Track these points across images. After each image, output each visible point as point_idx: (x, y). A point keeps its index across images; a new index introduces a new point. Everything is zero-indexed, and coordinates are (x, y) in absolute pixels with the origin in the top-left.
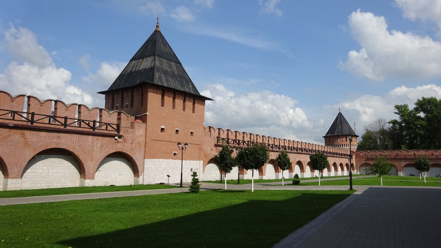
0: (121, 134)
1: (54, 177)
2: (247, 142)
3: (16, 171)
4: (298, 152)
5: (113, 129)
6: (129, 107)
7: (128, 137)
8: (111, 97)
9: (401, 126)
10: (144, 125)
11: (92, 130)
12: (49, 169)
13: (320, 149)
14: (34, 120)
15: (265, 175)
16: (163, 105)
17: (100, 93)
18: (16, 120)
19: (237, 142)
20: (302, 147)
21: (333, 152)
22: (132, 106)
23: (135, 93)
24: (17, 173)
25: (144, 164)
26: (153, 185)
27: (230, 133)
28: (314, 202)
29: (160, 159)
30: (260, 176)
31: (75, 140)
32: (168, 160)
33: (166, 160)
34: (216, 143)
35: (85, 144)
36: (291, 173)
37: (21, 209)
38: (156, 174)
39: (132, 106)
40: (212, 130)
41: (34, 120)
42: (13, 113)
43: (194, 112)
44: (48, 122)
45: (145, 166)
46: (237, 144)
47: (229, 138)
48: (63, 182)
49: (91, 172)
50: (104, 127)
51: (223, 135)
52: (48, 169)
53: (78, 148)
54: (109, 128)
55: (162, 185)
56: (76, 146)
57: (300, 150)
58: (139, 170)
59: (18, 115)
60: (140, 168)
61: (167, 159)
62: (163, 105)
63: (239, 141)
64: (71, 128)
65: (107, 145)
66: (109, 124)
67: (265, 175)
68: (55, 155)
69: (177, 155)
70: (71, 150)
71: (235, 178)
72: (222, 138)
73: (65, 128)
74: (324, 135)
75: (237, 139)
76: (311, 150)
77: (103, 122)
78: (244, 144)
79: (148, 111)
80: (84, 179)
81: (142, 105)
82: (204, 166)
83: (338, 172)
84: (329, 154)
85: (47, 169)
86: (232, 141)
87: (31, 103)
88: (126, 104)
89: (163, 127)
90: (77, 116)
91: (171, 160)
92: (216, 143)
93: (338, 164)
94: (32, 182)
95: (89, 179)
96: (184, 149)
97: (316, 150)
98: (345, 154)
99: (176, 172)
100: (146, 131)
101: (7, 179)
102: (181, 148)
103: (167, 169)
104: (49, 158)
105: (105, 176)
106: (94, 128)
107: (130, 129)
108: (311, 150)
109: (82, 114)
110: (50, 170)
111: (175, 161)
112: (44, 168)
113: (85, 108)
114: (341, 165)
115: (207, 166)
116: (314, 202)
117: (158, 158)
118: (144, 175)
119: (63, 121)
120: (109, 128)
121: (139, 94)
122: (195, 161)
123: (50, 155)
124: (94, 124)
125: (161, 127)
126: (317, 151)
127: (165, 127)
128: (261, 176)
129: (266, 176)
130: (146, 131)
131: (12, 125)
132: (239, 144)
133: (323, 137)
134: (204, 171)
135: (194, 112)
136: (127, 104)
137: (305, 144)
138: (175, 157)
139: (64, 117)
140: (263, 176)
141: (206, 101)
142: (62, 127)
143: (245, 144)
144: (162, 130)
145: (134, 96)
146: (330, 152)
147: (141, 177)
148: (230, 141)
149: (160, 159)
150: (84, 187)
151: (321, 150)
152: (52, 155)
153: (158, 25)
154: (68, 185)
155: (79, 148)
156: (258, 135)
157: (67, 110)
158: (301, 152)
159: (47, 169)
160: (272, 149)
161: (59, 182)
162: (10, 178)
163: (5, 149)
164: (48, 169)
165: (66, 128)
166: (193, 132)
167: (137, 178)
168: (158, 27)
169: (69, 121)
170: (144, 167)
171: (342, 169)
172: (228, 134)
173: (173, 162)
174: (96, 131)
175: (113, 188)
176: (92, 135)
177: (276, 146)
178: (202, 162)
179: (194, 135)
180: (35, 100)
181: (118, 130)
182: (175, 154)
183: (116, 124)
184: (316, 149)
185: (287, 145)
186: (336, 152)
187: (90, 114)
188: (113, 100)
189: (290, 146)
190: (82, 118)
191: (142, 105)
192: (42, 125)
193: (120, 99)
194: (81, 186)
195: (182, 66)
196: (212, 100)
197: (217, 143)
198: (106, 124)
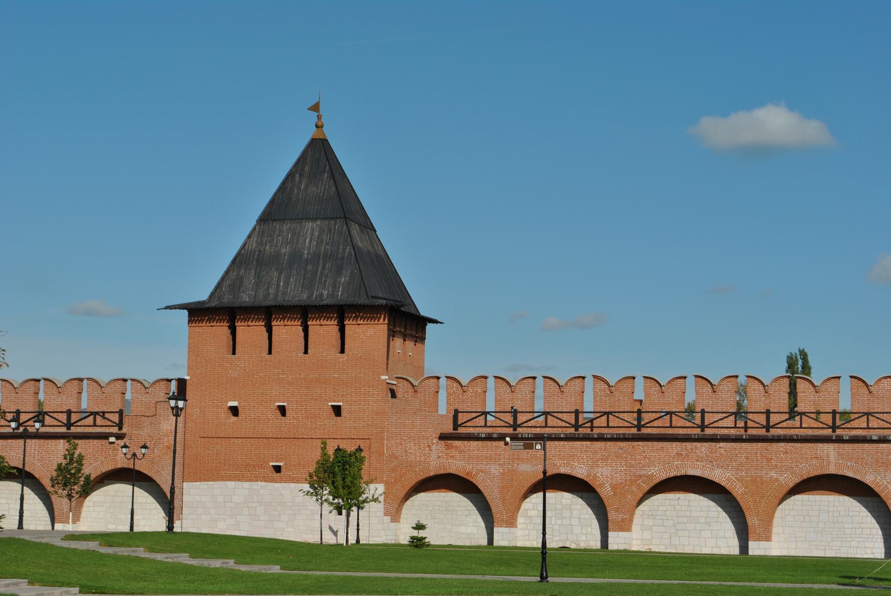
7: (142, 436)
12: (9, 504)
14: (580, 424)
26: (446, 545)
29: (227, 482)
31: (33, 450)
33: (248, 483)
35: (51, 457)
37: (210, 572)
38: (217, 516)
41: (72, 422)
43: (270, 353)
44: (92, 423)
49: (65, 510)
52: (850, 516)
53: (39, 464)
56: (34, 462)
61: (249, 481)
65: (94, 455)
69: (283, 470)
88: (398, 351)
89: (235, 404)
91: (263, 484)
95: (61, 523)
99: (279, 515)
103: (250, 505)
104: (117, 483)
105: (112, 520)
107: (146, 418)
113: (95, 383)
115: (780, 506)
117: (223, 480)
119: (762, 419)
125: (227, 405)
127: (239, 403)
131: (848, 438)
135: (270, 353)
139: (118, 410)
144: (235, 411)
149: (227, 482)
153: (320, 124)
155: (40, 465)
157: (60, 393)
159: (7, 503)
162: (611, 531)
164: (850, 516)
165: (515, 432)
166: (340, 406)
168: (322, 127)
173: (270, 488)
176: (63, 439)
182: (278, 469)
187: (104, 394)
196: (441, 323)
197: (455, 428)
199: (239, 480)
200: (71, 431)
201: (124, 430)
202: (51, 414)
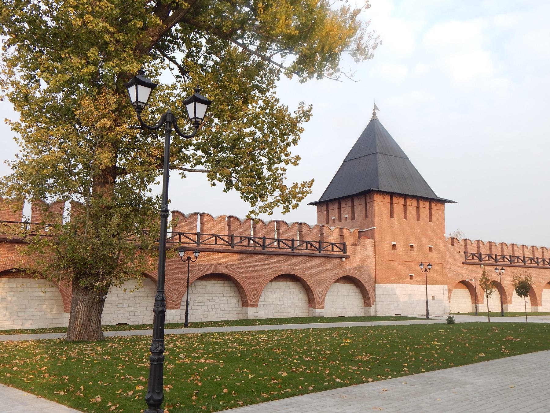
0: (348, 254)
1: (285, 306)
2: (509, 258)
6: (349, 220)
8: (324, 208)
9: (136, 73)
10: (371, 241)
11: (196, 245)
15: (541, 305)
16: (392, 215)
17: (310, 204)
18: (281, 248)
22: (353, 218)
25: (375, 291)
27: (481, 245)
30: (533, 307)
34: (464, 261)
38: (390, 302)
39: (353, 218)
40: (455, 242)
43: (430, 220)
44: (331, 250)
45: (377, 293)
46: (493, 260)
47: (526, 256)
48: (293, 311)
51: (472, 250)
55: (397, 317)
57: (475, 258)
58: (371, 298)
59: (289, 245)
60: (371, 295)
62: (392, 215)
63: (496, 255)
64: (325, 252)
66: (182, 234)
67: (541, 305)
69: (414, 278)
70: (299, 275)
71: (494, 310)
78: (544, 263)
79: (376, 224)
81: (366, 217)
82: (450, 291)
86: (471, 255)
87: (205, 221)
88: (345, 216)
89: (394, 243)
90: (276, 236)
91: (407, 285)
92: (464, 261)
94: (266, 311)
96: (428, 270)
100: (375, 249)
101: (246, 308)
102: (424, 270)
106: (293, 248)
109: (304, 233)
110: (281, 299)
112: (276, 296)
118: (376, 304)
119: (290, 243)
122: (437, 286)
124: (293, 244)
128: (536, 307)
129: (543, 306)
130: (375, 249)
132: (496, 260)
134: (449, 299)
135: (430, 220)
136: (347, 216)
137: (523, 248)
138: (411, 280)
140: (508, 305)
142: (317, 252)
143: (506, 260)
145: (355, 207)
147: (373, 306)
154: (298, 314)
156: (525, 246)
160: (538, 265)
161: (289, 311)
169: (267, 242)
170: (375, 295)
174: (295, 251)
175: (341, 318)
177: (518, 258)
178: (446, 287)
179: (434, 251)
181: (344, 250)
184: (524, 254)
185: (528, 254)
188: (328, 211)
189: (494, 253)
190: (305, 239)
191: (366, 217)
192: (272, 250)
193: (337, 210)
195: (409, 161)
196: (454, 202)
197: (465, 260)
199: (398, 283)
200: (234, 249)
202: (284, 241)
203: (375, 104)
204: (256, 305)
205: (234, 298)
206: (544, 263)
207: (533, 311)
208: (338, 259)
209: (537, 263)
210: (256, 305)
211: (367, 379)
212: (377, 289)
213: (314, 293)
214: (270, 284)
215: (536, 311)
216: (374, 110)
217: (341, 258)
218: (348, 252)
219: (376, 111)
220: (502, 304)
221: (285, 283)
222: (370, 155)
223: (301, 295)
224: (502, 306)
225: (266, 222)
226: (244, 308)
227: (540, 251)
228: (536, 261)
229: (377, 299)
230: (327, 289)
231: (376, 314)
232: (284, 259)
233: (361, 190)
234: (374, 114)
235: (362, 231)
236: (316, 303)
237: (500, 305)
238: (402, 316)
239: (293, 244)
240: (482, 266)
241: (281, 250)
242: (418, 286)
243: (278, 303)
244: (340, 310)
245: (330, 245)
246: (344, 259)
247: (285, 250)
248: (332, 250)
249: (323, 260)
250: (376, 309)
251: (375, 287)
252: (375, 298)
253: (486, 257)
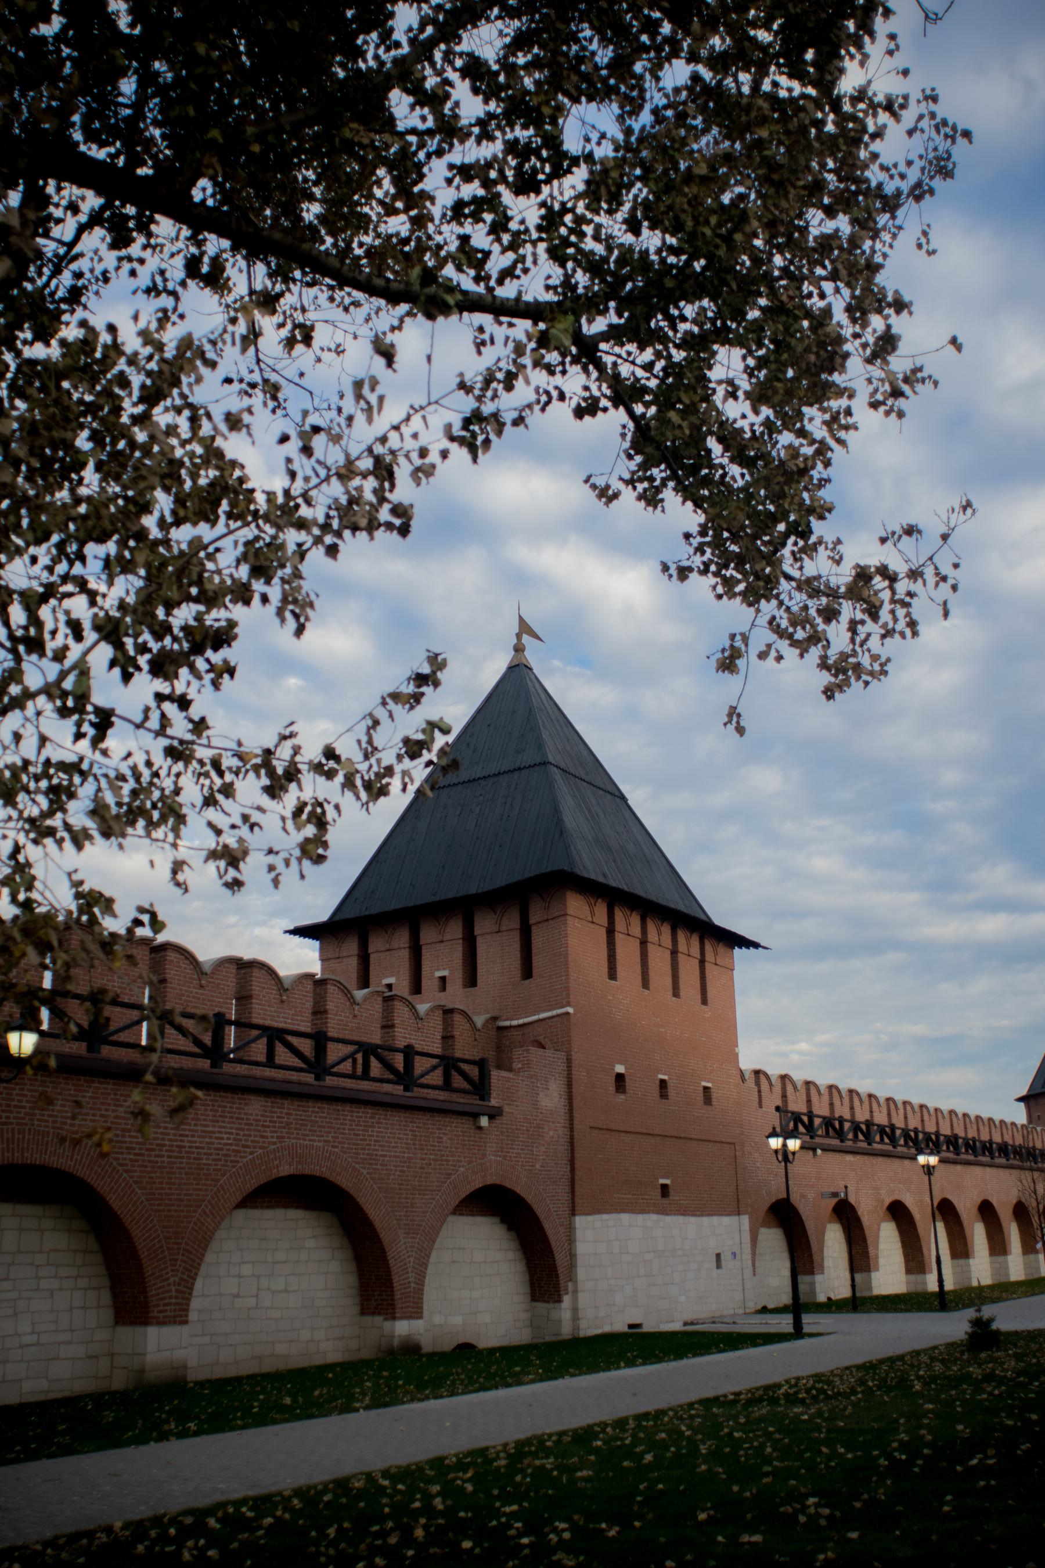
0: (494, 1102)
3: (173, 1288)
4: (875, 1146)
5: (296, 1062)
12: (258, 1277)
13: (1008, 1139)
19: (399, 1060)
20: (894, 1121)
21: (841, 1120)
23: (483, 925)
24: (177, 1298)
25: (571, 1240)
28: (757, 1538)
30: (912, 1277)
32: (646, 1216)
36: (1000, 1259)
42: (359, 1057)
43: (704, 1001)
44: (262, 1058)
50: (259, 1050)
54: (282, 1055)
57: (886, 1140)
68: (278, 1207)
69: (672, 1192)
72: (268, 1023)
73: (215, 1070)
74: (1024, 1092)
75: (401, 1043)
76: (863, 1127)
77: (257, 1020)
78: (856, 1136)
80: (386, 1319)
81: (527, 972)
83: (874, 1275)
84: (882, 1139)
85: (253, 1275)
89: (620, 1069)
93: (867, 1207)
94: (207, 1340)
97: (811, 1116)
98: (869, 1123)
101: (139, 1330)
106: (215, 1052)
108: (863, 1127)
111: (668, 1219)
112: (247, 1270)
114: (986, 1210)
116: (757, 1538)
118: (576, 1291)
120: (282, 1055)
121: (503, 928)
123: (262, 1207)
124: (218, 1036)
126: (817, 1121)
128: (919, 1277)
133: (1020, 1100)
135: (704, 1001)
136: (445, 973)
138: (665, 1201)
141: (737, 950)
146: (893, 1127)
147: (567, 1299)
148: (334, 1052)
150: (970, 1289)
151: (847, 1115)
152: (268, 1207)
158: (890, 1148)
159: (253, 1275)
163: (136, 1182)
167: (551, 1305)
171: (998, 1246)
172: (326, 1012)
174: (227, 1068)
178: (745, 1220)
180: (184, 964)
183: (309, 1030)
186: (867, 1116)
191: (527, 972)
194: (1030, 1277)
196: (756, 945)
198: (264, 1029)
199: (633, 1212)
201: (494, 1102)
203: (520, 618)
204: (180, 1317)
205: (83, 1283)
206: (856, 1136)
207: (912, 1289)
208: (567, 1131)
209: (406, 1078)
210: (180, 1317)
211: (237, 1510)
212: (579, 1234)
213: (390, 1254)
214: (240, 1214)
215: (919, 1289)
216: (519, 636)
217: (475, 1116)
218: (494, 1095)
219: (526, 639)
220: (853, 1270)
221: (279, 1213)
222: (520, 769)
223: (335, 1266)
224: (853, 1280)
225: (206, 962)
226: (126, 1332)
227: (826, 1098)
228: (401, 1067)
229: (581, 1273)
230: (431, 1237)
231: (576, 1328)
232: (289, 1110)
233: (502, 880)
234: (519, 649)
235: (507, 1023)
236: (398, 1295)
237: (847, 1275)
238: (646, 1329)
239: (409, 1063)
240: (819, 1152)
241: (280, 1074)
242: (681, 1219)
243: (252, 1302)
244: (458, 1320)
245: (258, 1038)
246: (484, 1121)
247: (294, 1076)
248: (270, 1061)
249: (420, 1123)
250: (575, 1310)
251: (571, 1229)
252: (572, 1265)
253: (434, 1068)
